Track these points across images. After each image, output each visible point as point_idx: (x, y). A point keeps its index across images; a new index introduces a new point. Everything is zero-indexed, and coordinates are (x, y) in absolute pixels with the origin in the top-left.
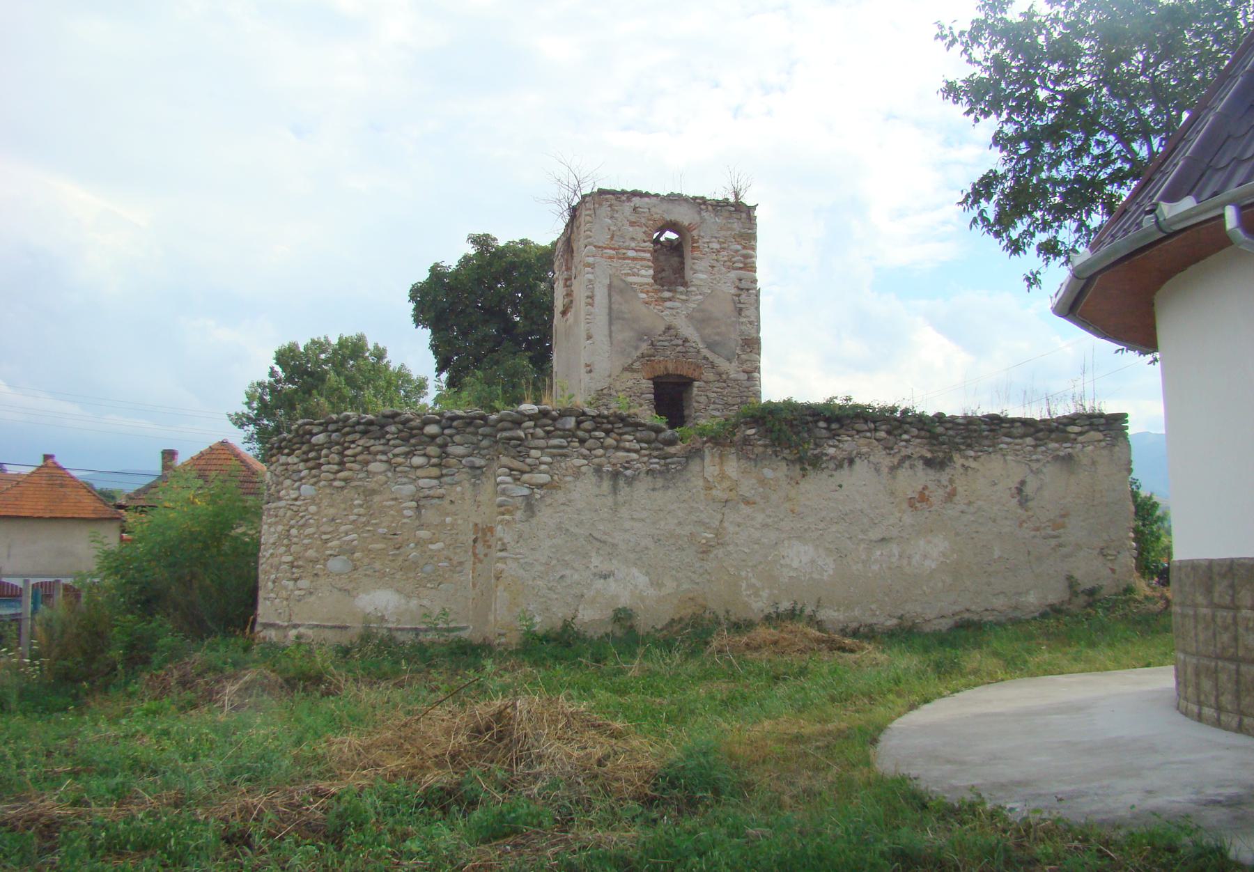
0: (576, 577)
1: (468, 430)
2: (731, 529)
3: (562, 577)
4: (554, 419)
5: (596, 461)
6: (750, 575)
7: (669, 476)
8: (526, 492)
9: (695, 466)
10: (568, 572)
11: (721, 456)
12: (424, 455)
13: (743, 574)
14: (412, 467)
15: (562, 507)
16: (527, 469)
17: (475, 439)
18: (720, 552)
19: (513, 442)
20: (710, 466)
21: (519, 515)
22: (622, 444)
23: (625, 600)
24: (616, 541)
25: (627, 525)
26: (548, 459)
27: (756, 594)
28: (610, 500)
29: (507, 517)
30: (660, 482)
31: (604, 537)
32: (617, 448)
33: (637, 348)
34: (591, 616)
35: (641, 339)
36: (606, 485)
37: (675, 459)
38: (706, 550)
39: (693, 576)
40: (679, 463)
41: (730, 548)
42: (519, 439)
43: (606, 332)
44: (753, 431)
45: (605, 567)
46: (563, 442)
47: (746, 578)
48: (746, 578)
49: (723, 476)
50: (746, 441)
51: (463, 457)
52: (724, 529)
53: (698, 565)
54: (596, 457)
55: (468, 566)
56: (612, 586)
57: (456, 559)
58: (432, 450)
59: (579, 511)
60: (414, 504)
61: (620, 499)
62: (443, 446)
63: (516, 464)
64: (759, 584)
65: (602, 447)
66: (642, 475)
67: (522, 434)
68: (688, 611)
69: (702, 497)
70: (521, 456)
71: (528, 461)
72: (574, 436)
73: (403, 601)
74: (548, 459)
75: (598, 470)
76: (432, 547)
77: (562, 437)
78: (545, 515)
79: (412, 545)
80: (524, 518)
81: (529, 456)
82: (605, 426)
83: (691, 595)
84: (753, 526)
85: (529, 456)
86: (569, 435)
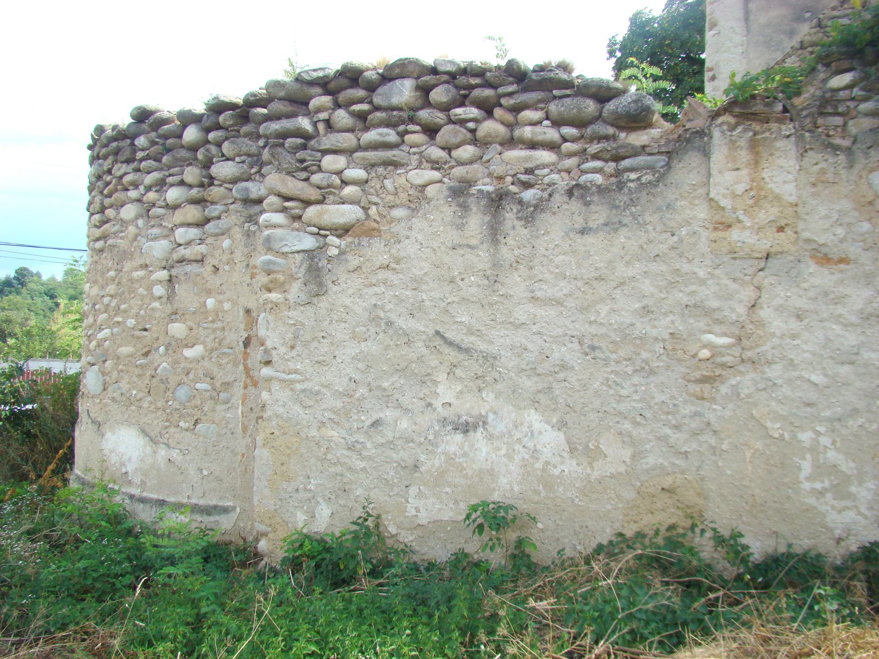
0: (404, 424)
1: (245, 129)
2: (777, 324)
3: (376, 424)
4: (372, 87)
5: (458, 171)
6: (825, 441)
7: (622, 199)
8: (309, 242)
9: (686, 172)
10: (388, 414)
11: (754, 145)
12: (182, 183)
13: (806, 437)
14: (167, 206)
15: (382, 275)
16: (314, 194)
17: (252, 146)
18: (746, 381)
19: (290, 142)
20: (724, 170)
21: (296, 290)
22: (517, 133)
23: (507, 486)
24: (493, 349)
25: (521, 314)
26: (358, 173)
27: (840, 490)
28: (482, 258)
29: (274, 296)
30: (599, 214)
31: (469, 341)
32: (510, 142)
33: (791, 34)
34: (425, 516)
35: (799, 19)
36: (476, 222)
37: (641, 160)
38: (709, 377)
39: (676, 437)
40: (651, 168)
41: (775, 372)
42: (299, 133)
43: (740, 14)
44: (846, 78)
45: (468, 406)
46: (391, 136)
47: (814, 449)
48: (814, 449)
49: (758, 195)
50: (828, 104)
51: (235, 181)
52: (761, 324)
53: (688, 409)
54: (460, 163)
55: (238, 390)
56: (481, 450)
57: (221, 377)
58: (192, 174)
59: (417, 284)
60: (163, 274)
61: (506, 253)
62: (207, 164)
63: (294, 186)
64: (847, 466)
65: (475, 141)
66: (558, 199)
67: (305, 123)
68: (659, 517)
69: (703, 246)
70: (306, 169)
71: (316, 178)
72: (412, 120)
73: (149, 450)
74: (358, 173)
75: (460, 191)
76: (188, 353)
77: (388, 125)
78: (348, 293)
79: (162, 349)
80: (303, 297)
81: (320, 170)
82: (477, 93)
83: (668, 482)
84: (837, 319)
85: (320, 170)
86: (400, 118)
